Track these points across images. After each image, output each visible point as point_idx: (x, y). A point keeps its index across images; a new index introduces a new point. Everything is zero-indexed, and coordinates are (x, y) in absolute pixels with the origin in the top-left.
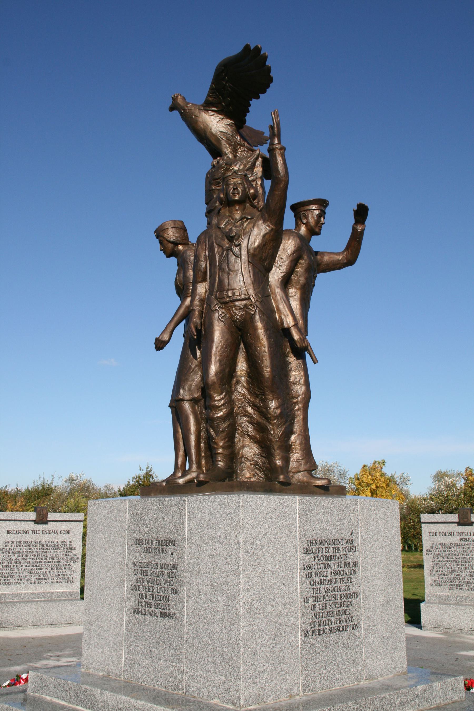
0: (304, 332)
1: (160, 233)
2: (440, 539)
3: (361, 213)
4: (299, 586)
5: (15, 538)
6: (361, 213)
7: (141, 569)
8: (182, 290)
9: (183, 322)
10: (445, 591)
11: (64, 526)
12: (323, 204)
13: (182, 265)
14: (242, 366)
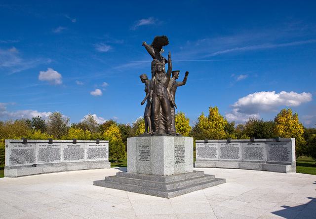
0: (174, 101)
1: (141, 77)
2: (200, 146)
3: (187, 73)
4: (173, 154)
5: (92, 147)
6: (187, 73)
7: (141, 152)
8: (146, 91)
9: (311, 200)
10: (200, 158)
11: (104, 144)
12: (179, 71)
13: (147, 85)
14: (161, 109)
